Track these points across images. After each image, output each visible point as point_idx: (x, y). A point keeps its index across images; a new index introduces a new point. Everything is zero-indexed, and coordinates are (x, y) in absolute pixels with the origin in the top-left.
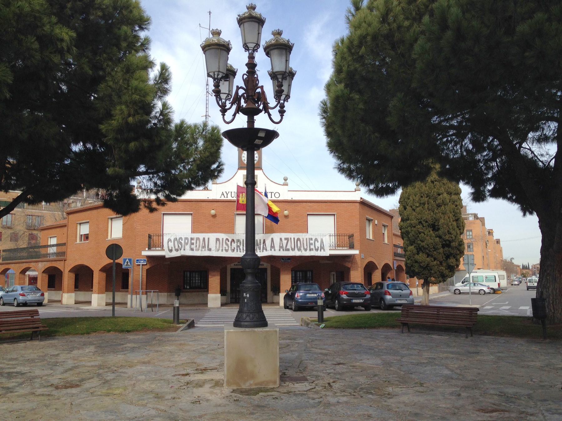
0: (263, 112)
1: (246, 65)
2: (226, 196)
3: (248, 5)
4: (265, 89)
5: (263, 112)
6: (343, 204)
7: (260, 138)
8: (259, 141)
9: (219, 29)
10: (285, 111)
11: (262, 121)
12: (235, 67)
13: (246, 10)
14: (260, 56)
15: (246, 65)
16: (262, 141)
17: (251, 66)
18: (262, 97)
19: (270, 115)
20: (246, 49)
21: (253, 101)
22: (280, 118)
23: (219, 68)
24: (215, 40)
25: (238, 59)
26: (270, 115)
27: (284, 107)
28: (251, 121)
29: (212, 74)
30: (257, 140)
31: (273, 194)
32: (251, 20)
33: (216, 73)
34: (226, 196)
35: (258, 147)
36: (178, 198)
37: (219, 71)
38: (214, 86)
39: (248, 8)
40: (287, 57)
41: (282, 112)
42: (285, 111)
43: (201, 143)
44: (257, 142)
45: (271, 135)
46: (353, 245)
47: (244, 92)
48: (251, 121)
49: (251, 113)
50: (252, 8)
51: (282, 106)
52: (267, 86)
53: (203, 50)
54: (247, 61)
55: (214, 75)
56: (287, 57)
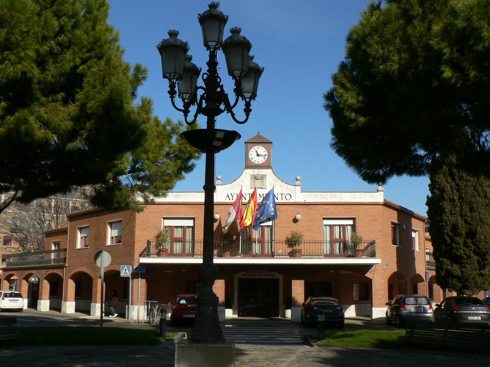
0: (226, 112)
1: (207, 63)
2: (231, 198)
3: (210, 4)
4: (224, 88)
5: (226, 112)
6: (364, 206)
7: (219, 140)
8: (218, 142)
9: (176, 30)
10: (251, 110)
11: (223, 122)
12: (198, 66)
13: (208, 8)
14: (221, 56)
15: (207, 63)
16: (221, 143)
17: (212, 64)
18: (224, 98)
19: (233, 115)
20: (207, 48)
21: (215, 102)
22: (245, 117)
23: (175, 69)
24: (172, 41)
25: (199, 57)
26: (233, 115)
27: (250, 105)
28: (211, 122)
29: (167, 75)
30: (215, 142)
31: (284, 196)
32: (212, 19)
33: (172, 74)
34: (231, 198)
35: (218, 150)
36: (158, 200)
37: (175, 73)
38: (170, 87)
39: (210, 6)
40: (192, 81)
41: (248, 111)
42: (251, 110)
43: (114, 155)
44: (215, 143)
45: (230, 137)
46: (375, 253)
47: (204, 92)
48: (211, 122)
49: (212, 113)
50: (213, 6)
51: (248, 105)
52: (228, 84)
53: (159, 51)
54: (207, 59)
55: (170, 75)
56: (192, 81)
